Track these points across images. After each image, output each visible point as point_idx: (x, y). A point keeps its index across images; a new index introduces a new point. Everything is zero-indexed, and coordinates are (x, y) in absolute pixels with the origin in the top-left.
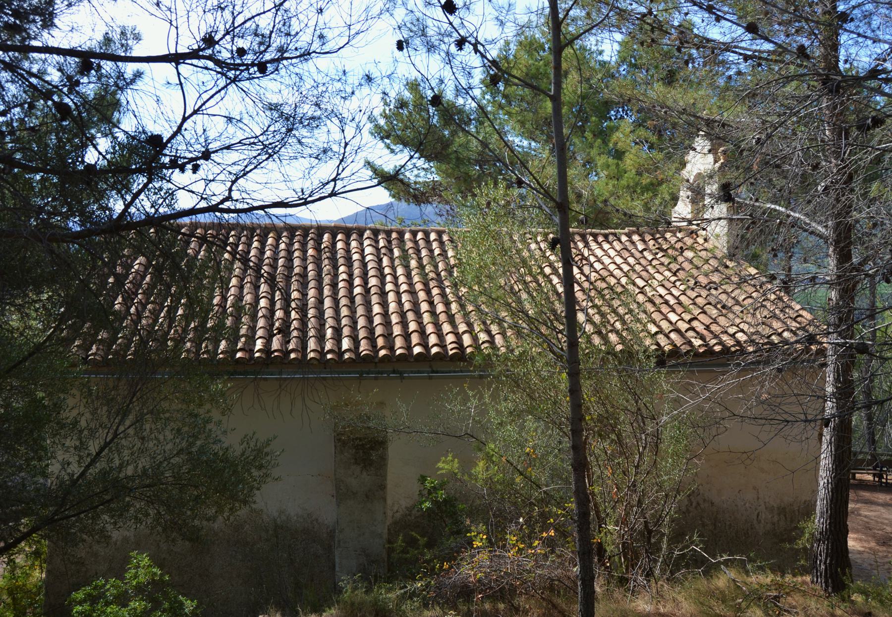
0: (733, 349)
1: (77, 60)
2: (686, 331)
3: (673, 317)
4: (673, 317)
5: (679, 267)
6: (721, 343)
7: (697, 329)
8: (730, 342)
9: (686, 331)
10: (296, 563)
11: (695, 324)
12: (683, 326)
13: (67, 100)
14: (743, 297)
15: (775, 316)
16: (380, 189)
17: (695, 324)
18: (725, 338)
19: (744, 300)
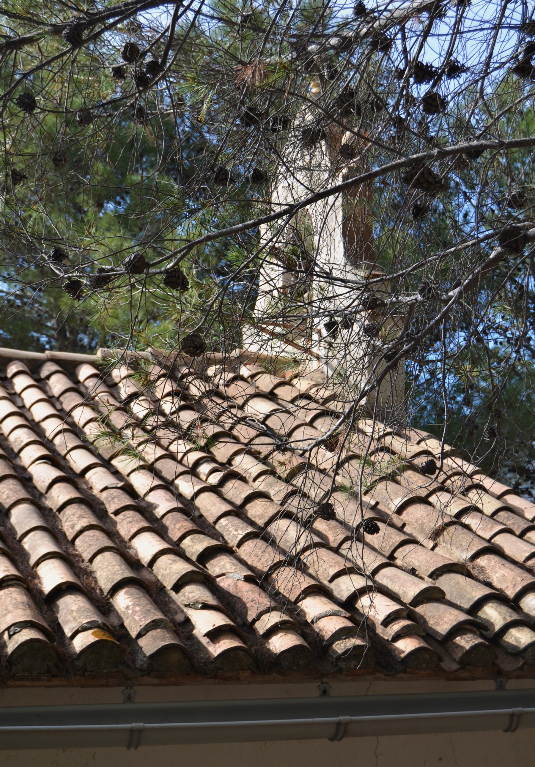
0: (340, 647)
1: (403, 655)
2: (178, 587)
3: (146, 546)
4: (146, 546)
5: (296, 461)
6: (297, 624)
7: (224, 583)
8: (328, 622)
9: (178, 587)
10: (528, 26)
11: (218, 566)
12: (170, 570)
13: (451, 104)
14: (398, 501)
15: (492, 550)
16: (214, 575)
17: (218, 566)
18: (313, 607)
19: (400, 511)
